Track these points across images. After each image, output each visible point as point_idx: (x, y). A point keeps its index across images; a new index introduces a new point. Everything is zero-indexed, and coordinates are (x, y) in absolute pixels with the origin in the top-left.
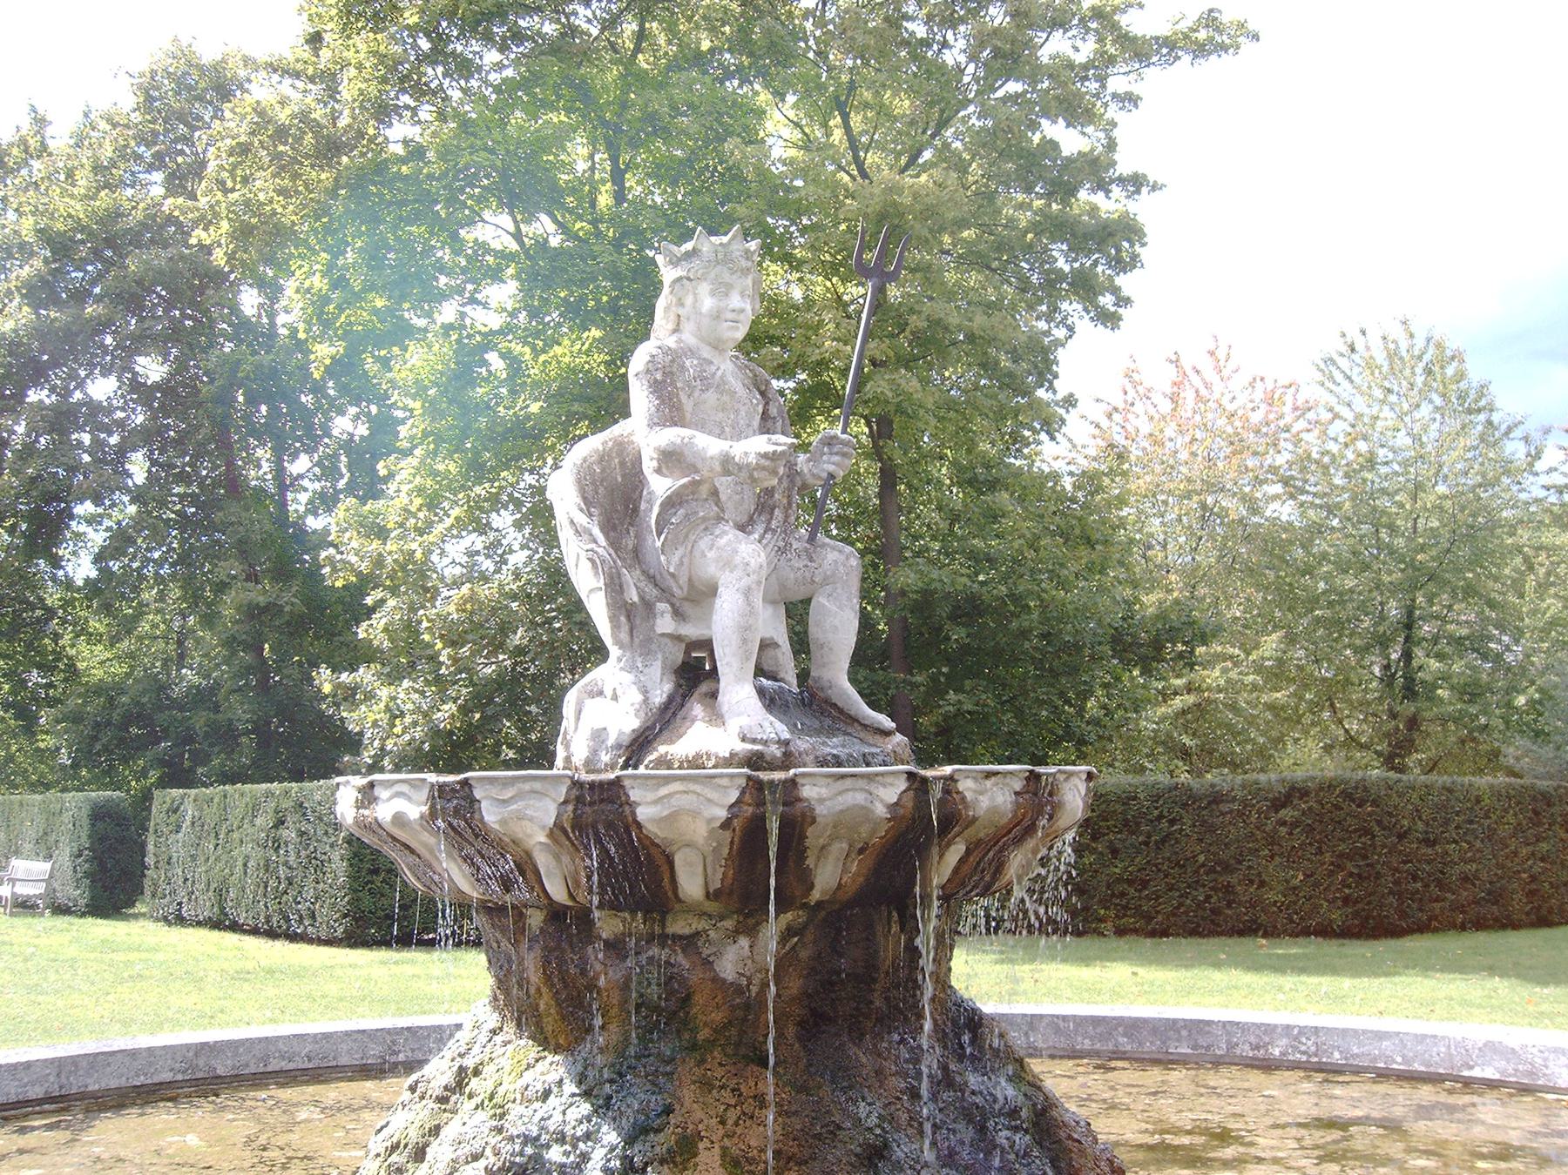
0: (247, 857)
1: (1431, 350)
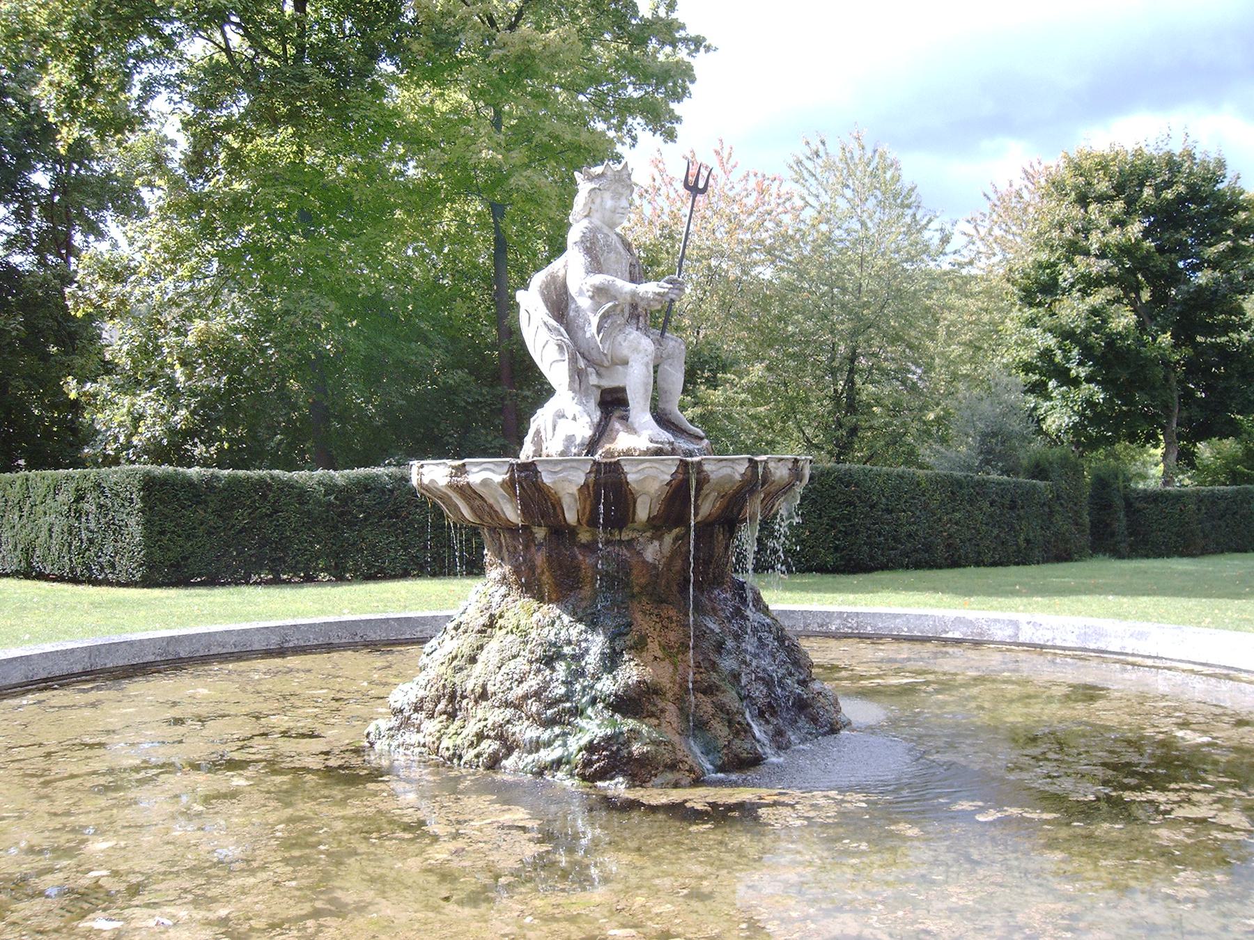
0: (52, 525)
1: (877, 159)
